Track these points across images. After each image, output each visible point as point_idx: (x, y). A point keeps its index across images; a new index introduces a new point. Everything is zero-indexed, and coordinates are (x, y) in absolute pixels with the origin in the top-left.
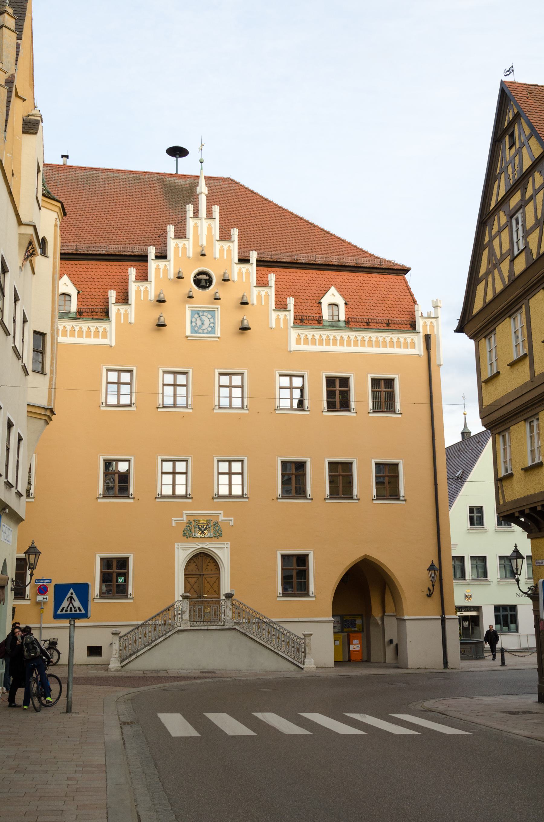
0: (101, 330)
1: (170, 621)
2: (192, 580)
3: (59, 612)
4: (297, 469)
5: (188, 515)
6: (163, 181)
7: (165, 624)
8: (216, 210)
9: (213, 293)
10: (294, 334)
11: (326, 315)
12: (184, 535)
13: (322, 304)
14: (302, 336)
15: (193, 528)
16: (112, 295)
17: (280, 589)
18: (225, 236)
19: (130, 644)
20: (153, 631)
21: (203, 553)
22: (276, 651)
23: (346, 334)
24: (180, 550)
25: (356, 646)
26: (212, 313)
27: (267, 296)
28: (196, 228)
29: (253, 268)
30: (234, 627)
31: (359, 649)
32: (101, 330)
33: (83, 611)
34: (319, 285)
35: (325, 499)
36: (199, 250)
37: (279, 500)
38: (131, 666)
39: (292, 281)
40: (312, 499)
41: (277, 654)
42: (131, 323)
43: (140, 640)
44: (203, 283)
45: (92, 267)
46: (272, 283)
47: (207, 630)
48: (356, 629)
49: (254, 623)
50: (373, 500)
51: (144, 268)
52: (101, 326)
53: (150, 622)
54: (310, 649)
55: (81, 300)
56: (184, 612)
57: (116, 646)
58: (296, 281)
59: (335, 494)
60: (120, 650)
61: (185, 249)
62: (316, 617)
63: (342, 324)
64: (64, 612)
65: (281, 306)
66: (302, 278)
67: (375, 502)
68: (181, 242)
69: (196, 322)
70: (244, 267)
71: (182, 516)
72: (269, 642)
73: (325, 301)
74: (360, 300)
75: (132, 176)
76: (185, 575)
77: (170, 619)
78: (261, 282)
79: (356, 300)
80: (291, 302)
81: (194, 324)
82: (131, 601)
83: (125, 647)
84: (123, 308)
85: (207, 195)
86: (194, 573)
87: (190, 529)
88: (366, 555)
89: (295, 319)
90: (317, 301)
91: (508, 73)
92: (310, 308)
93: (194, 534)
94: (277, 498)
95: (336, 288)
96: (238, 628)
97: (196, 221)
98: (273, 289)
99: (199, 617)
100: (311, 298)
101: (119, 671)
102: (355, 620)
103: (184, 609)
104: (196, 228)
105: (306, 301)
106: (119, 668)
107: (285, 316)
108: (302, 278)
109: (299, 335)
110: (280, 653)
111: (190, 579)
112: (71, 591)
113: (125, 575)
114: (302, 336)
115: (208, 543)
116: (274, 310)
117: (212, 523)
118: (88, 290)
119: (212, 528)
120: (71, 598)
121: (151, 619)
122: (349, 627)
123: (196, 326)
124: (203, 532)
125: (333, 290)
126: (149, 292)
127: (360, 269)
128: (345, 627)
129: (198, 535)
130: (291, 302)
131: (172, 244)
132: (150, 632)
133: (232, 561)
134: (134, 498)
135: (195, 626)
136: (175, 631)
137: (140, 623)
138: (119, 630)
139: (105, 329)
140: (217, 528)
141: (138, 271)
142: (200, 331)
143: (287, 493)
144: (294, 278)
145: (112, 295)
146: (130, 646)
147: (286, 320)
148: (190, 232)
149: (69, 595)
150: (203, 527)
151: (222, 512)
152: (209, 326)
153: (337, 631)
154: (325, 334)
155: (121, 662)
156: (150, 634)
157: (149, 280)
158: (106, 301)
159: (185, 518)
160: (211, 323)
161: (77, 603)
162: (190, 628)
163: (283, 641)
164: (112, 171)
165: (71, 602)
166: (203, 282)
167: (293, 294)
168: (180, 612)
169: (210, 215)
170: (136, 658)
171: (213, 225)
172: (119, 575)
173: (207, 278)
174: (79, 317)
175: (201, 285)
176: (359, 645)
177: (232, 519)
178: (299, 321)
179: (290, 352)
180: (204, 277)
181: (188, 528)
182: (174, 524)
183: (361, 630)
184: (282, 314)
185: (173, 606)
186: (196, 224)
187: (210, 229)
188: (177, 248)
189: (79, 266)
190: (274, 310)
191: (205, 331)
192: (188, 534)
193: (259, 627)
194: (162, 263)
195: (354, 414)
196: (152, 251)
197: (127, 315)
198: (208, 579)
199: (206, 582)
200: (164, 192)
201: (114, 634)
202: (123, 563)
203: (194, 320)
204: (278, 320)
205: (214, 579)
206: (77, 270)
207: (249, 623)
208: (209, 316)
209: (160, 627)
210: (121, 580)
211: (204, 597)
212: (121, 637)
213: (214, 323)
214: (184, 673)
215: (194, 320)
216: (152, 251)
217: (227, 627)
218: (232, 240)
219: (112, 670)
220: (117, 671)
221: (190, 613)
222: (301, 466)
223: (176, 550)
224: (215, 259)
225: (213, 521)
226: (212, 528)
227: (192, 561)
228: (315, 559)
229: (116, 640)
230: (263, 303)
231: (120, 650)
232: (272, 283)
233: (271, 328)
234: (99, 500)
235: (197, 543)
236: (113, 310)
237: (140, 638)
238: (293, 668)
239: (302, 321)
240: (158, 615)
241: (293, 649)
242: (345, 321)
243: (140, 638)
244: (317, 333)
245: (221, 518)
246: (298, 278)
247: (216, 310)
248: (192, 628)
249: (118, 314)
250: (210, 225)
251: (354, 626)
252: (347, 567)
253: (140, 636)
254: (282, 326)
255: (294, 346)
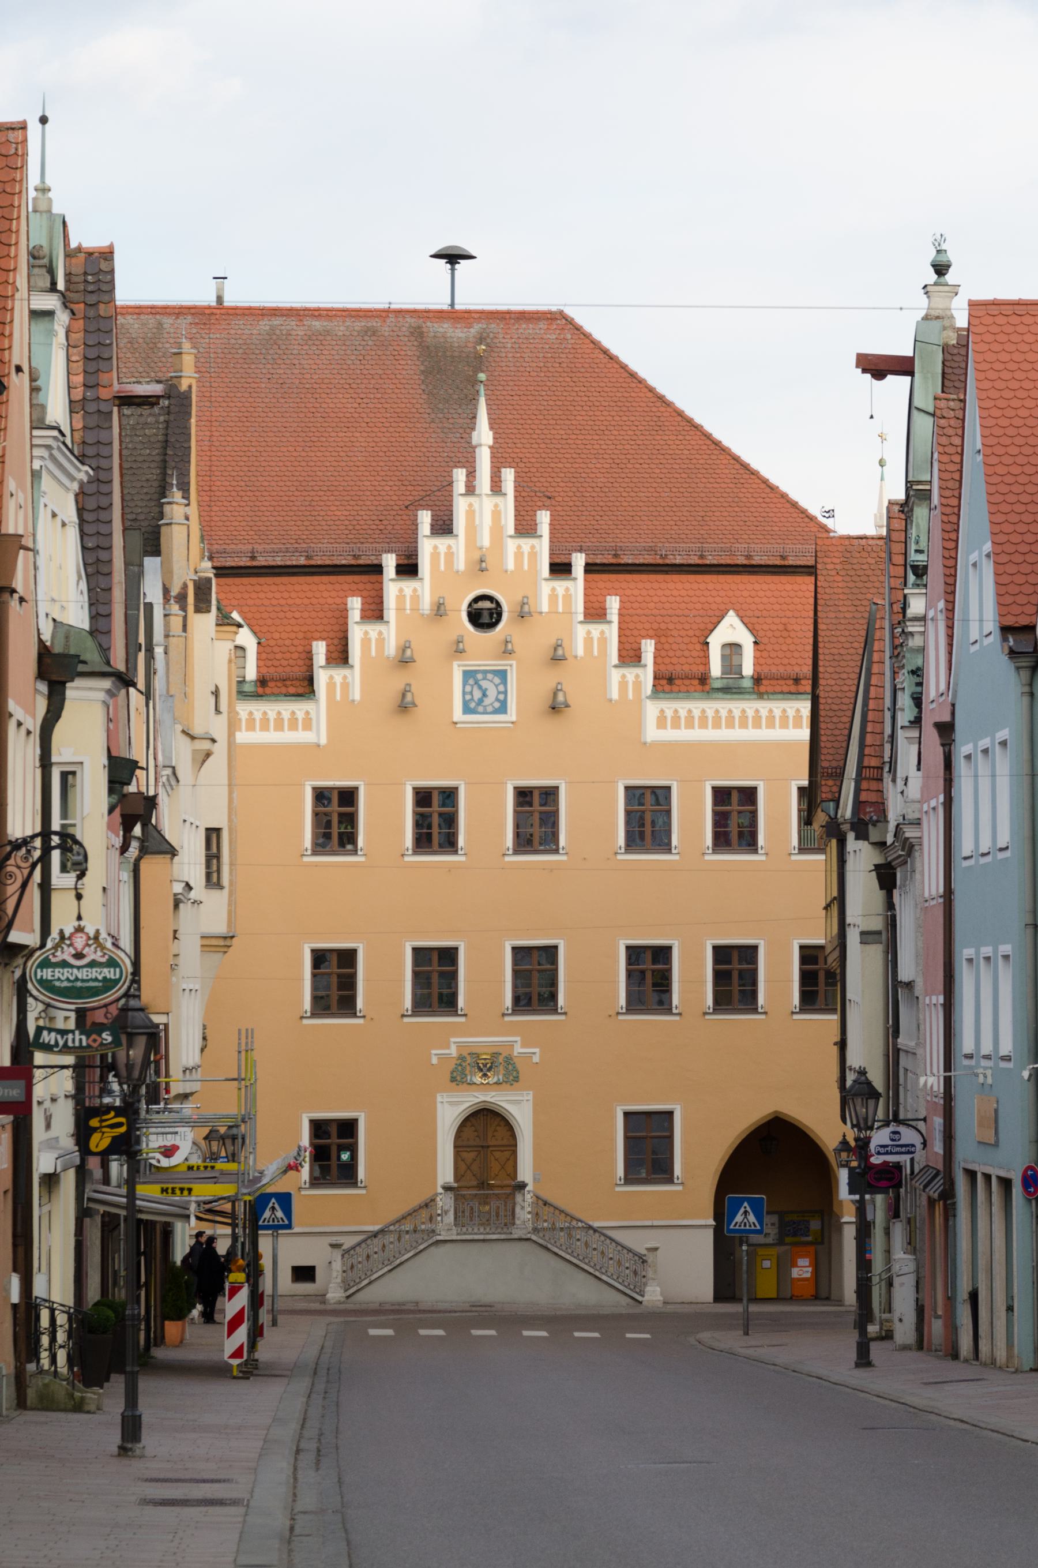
0: (300, 715)
1: (423, 1227)
2: (469, 1156)
3: (732, 1227)
4: (655, 961)
5: (459, 1048)
6: (421, 334)
7: (415, 1231)
8: (509, 476)
9: (502, 637)
10: (652, 709)
11: (716, 669)
12: (453, 1079)
13: (711, 646)
14: (669, 714)
15: (468, 1068)
16: (320, 650)
17: (620, 1171)
18: (525, 528)
19: (360, 1262)
20: (396, 1243)
21: (488, 1110)
22: (597, 1274)
23: (750, 706)
24: (446, 1105)
25: (802, 1270)
26: (502, 675)
27: (603, 640)
28: (471, 513)
29: (577, 584)
30: (529, 1236)
31: (808, 1275)
32: (300, 715)
33: (758, 1227)
34: (706, 606)
35: (705, 1014)
36: (477, 556)
37: (621, 1017)
38: (360, 1297)
39: (656, 599)
40: (680, 1014)
41: (600, 1279)
42: (353, 701)
43: (376, 1256)
44: (485, 619)
45: (282, 588)
46: (613, 614)
47: (484, 1241)
48: (810, 1239)
49: (562, 1229)
50: (793, 1013)
51: (376, 587)
52: (299, 708)
53: (392, 1228)
54: (655, 1272)
55: (264, 656)
56: (446, 1212)
57: (338, 1265)
58: (664, 599)
59: (723, 1001)
60: (344, 1272)
61: (450, 555)
62: (683, 1218)
63: (747, 684)
64: (737, 1227)
65: (630, 656)
66: (675, 593)
67: (795, 1017)
68: (443, 543)
69: (471, 693)
70: (561, 586)
71: (448, 1047)
72: (587, 1261)
73: (716, 640)
74: (785, 634)
75: (359, 325)
76: (455, 1147)
77: (423, 1223)
78: (592, 611)
79: (777, 634)
80: (648, 647)
81: (468, 697)
82: (363, 1192)
83: (352, 1267)
84: (338, 674)
85: (490, 447)
86: (472, 1143)
87: (464, 1069)
88: (776, 1112)
89: (655, 678)
90: (702, 639)
91: (827, 515)
92: (687, 653)
93: (469, 1078)
94: (618, 1013)
95: (737, 612)
96: (534, 1237)
97: (471, 499)
98: (615, 626)
99: (471, 1220)
100: (691, 633)
101: (343, 1303)
102: (808, 1222)
103: (446, 1208)
104: (471, 513)
105: (680, 640)
106: (343, 1300)
107: (637, 676)
108: (675, 593)
109: (662, 711)
110: (604, 1277)
111: (464, 1155)
112: (273, 1200)
113: (353, 1150)
114: (669, 714)
115: (494, 1093)
116: (615, 666)
117: (501, 1059)
118: (276, 636)
119: (501, 1068)
120: (273, 1208)
121: (393, 1224)
122: (795, 1235)
123: (472, 699)
124: (485, 1075)
125: (731, 619)
126: (386, 642)
127: (789, 570)
128: (788, 1235)
129: (478, 1079)
130: (648, 647)
131: (428, 547)
132: (391, 1243)
133: (537, 1125)
134: (364, 1017)
135: (465, 1234)
136: (431, 1241)
137: (376, 1228)
138: (340, 1239)
139: (307, 713)
140: (510, 1067)
141: (367, 607)
142: (480, 709)
143: (636, 1003)
144: (660, 592)
145: (320, 650)
146: (360, 1266)
147: (638, 684)
148: (460, 523)
149: (271, 1205)
150: (485, 1065)
151: (518, 1039)
152: (497, 700)
153: (771, 1242)
154: (711, 707)
155: (346, 1291)
156: (392, 1246)
157: (385, 619)
158: (309, 657)
159: (453, 1051)
160: (499, 693)
161: (280, 1214)
162: (455, 1238)
163: (611, 1259)
164: (316, 313)
165: (273, 1213)
166: (486, 614)
167: (651, 632)
168: (439, 1212)
169: (496, 487)
170: (370, 1283)
171: (502, 507)
172: (341, 1148)
173: (493, 606)
174: (260, 690)
175: (481, 621)
176: (810, 1269)
177: (537, 1050)
178: (664, 682)
179: (645, 743)
180: (487, 604)
181: (460, 1068)
182: (434, 1061)
183: (820, 1240)
184: (631, 674)
185: (433, 1200)
186: (471, 505)
187: (496, 514)
188: (435, 555)
189: (258, 588)
190: (615, 666)
191: (490, 709)
192: (458, 1078)
193: (570, 1236)
194: (408, 586)
195: (763, 858)
196: (390, 562)
197: (346, 686)
198: (497, 1154)
199: (493, 1158)
200: (423, 372)
201: (335, 1246)
202: (348, 1127)
203: (468, 689)
204: (623, 684)
205: (507, 1154)
206: (254, 595)
207: (553, 1229)
208: (497, 680)
209: (407, 1236)
210: (345, 1156)
211: (491, 1187)
212: (347, 1251)
213: (505, 693)
214: (441, 1306)
215: (468, 689)
216: (390, 562)
217: (516, 1236)
218: (539, 533)
219: (332, 1301)
220: (339, 1303)
221: (456, 1213)
222: (662, 954)
223: (439, 1105)
224: (506, 571)
225: (504, 1055)
226: (501, 1068)
227: (469, 1124)
228: (684, 1118)
229: (337, 1255)
230: (596, 653)
231: (344, 1272)
232: (613, 614)
233: (611, 700)
234: (305, 1022)
235: (475, 1094)
236: (322, 677)
237: (376, 1253)
238: (624, 1300)
239: (670, 680)
240: (404, 1218)
241: (627, 1271)
242: (752, 677)
243: (376, 1253)
244: (697, 706)
245: (518, 1049)
246: (667, 593)
247: (508, 668)
248: (459, 1237)
249: (331, 685)
250: (496, 506)
251: (807, 1232)
252: (743, 1132)
253: (376, 1250)
254: (630, 696)
255: (652, 733)
